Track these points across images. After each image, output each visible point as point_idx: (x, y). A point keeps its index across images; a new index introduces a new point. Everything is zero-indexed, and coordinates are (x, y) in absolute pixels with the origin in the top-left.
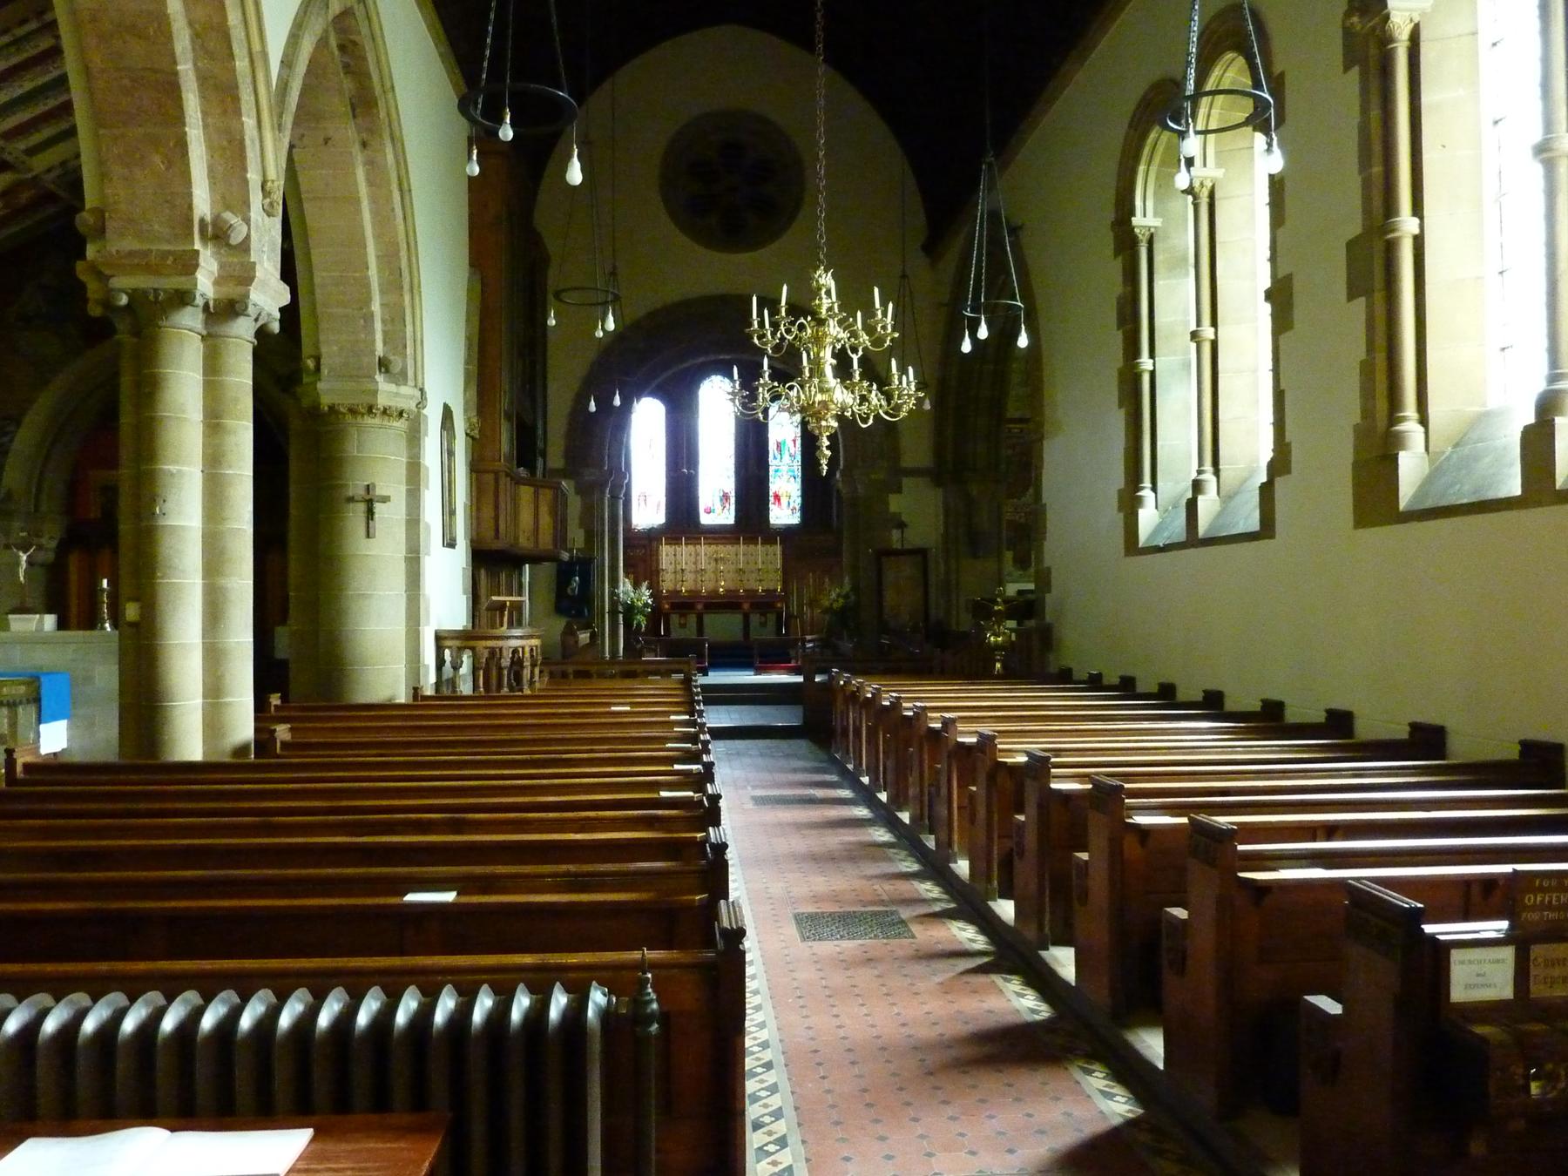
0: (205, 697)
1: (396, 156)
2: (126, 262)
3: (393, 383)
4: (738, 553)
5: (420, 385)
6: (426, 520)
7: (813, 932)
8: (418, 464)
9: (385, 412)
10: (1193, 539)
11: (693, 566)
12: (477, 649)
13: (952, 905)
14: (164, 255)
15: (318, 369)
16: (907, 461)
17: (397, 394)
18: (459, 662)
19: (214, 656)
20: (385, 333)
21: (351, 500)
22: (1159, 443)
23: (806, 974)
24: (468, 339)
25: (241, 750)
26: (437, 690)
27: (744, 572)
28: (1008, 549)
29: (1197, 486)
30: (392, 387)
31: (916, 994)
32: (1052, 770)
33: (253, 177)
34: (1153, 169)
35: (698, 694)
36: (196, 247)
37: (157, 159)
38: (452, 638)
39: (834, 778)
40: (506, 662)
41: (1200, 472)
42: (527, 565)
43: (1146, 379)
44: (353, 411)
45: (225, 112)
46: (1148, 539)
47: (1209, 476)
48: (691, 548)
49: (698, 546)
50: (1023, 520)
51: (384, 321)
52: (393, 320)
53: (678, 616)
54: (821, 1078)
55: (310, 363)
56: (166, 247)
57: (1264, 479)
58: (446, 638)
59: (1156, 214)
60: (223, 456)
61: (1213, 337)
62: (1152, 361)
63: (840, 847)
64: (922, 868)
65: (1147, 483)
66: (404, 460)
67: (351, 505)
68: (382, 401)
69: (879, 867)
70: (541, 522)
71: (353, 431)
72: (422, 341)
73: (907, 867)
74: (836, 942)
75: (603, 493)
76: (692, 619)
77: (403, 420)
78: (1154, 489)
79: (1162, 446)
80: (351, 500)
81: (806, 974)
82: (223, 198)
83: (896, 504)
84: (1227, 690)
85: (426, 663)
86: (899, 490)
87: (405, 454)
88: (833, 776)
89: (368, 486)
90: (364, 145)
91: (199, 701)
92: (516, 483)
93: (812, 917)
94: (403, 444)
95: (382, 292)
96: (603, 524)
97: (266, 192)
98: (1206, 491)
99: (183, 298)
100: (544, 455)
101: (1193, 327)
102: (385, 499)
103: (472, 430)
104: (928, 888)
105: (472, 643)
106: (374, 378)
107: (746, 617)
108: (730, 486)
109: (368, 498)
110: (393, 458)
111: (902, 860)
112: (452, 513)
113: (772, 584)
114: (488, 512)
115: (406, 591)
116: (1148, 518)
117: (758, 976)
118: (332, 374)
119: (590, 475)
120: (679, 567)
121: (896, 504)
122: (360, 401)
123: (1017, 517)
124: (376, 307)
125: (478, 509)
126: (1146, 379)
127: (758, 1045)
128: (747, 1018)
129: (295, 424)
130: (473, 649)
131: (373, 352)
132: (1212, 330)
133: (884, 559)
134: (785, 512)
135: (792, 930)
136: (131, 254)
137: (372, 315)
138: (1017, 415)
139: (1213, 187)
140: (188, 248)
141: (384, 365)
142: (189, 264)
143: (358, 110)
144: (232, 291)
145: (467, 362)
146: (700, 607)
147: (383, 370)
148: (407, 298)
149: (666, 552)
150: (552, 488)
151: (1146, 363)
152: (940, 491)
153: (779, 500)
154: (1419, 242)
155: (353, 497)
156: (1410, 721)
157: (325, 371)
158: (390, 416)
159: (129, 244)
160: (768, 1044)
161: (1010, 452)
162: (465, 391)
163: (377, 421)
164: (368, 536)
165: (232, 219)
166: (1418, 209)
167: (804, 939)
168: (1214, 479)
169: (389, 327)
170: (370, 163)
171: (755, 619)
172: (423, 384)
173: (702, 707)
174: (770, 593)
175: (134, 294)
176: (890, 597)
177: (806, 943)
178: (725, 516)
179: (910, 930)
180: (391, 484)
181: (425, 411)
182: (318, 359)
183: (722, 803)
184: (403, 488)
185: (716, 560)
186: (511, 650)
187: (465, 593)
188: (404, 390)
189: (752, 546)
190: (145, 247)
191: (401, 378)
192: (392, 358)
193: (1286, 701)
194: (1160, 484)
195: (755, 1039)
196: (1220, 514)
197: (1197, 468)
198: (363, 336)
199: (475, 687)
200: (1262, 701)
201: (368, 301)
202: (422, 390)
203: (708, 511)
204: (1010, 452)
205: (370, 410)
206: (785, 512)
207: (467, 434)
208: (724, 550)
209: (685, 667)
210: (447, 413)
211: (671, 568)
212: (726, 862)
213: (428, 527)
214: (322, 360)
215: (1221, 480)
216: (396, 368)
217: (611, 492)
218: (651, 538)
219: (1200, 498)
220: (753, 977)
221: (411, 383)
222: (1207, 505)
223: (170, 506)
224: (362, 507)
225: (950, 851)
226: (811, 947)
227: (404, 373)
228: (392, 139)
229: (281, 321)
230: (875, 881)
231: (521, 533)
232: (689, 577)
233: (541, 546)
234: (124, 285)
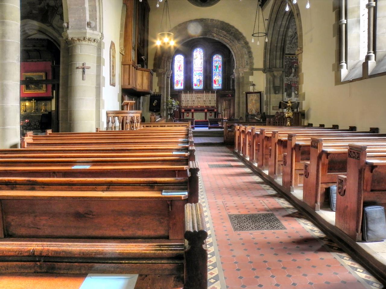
3: (91, 30)
4: (204, 96)
5: (101, 32)
6: (103, 75)
7: (239, 225)
9: (89, 40)
11: (191, 100)
12: (119, 117)
13: (296, 211)
15: (68, 27)
16: (255, 66)
17: (93, 34)
18: (114, 121)
20: (90, 15)
21: (77, 68)
22: (348, 47)
23: (239, 253)
24: (121, 24)
26: (107, 129)
27: (205, 101)
28: (285, 92)
29: (368, 58)
30: (91, 31)
31: (299, 267)
32: (367, 154)
39: (236, 158)
40: (128, 121)
41: (369, 53)
42: (142, 97)
43: (344, 26)
44: (79, 40)
47: (372, 54)
48: (190, 95)
49: (193, 94)
50: (289, 83)
51: (90, 11)
52: (92, 10)
53: (186, 113)
54: (237, 270)
55: (65, 25)
60: (6, 34)
62: (346, 20)
63: (243, 184)
64: (277, 193)
65: (344, 61)
66: (96, 56)
67: (78, 70)
68: (88, 36)
69: (260, 192)
70: (144, 81)
71: (79, 46)
72: (103, 18)
73: (271, 192)
74: (250, 232)
75: (164, 76)
76: (190, 114)
77: (95, 42)
78: (346, 63)
79: (349, 48)
80: (77, 68)
81: (239, 253)
83: (251, 79)
85: (103, 121)
86: (252, 74)
87: (96, 54)
88: (235, 158)
89: (83, 64)
92: (136, 69)
93: (237, 217)
94: (96, 50)
96: (164, 85)
98: (371, 59)
102: (89, 68)
103: (122, 51)
104: (282, 202)
106: (85, 28)
107: (206, 113)
108: (201, 78)
109: (83, 67)
110: (92, 55)
111: (268, 189)
112: (114, 76)
113: (213, 104)
114: (127, 77)
115: (96, 98)
116: (344, 72)
117: (213, 244)
118: (72, 28)
119: (160, 71)
120: (187, 100)
121: (251, 79)
122: (81, 36)
123: (288, 82)
125: (124, 76)
126: (344, 26)
127: (201, 198)
128: (208, 260)
129: (62, 45)
130: (118, 117)
131: (85, 20)
133: (248, 95)
134: (217, 85)
135: (228, 225)
137: (85, 8)
138: (288, 53)
141: (89, 24)
145: (121, 31)
146: (193, 110)
147: (89, 26)
149: (183, 96)
150: (148, 71)
151: (344, 21)
152: (265, 74)
153: (215, 82)
155: (78, 67)
157: (70, 27)
158: (91, 41)
160: (208, 222)
161: (286, 63)
162: (120, 40)
163: (87, 43)
167: (236, 229)
168: (374, 55)
171: (208, 114)
172: (103, 32)
173: (194, 148)
174: (213, 107)
176: (250, 106)
177: (236, 231)
178: (201, 87)
179: (282, 225)
181: (103, 41)
182: (68, 23)
183: (199, 174)
184: (95, 65)
185: (198, 98)
186: (130, 117)
187: (118, 101)
188: (95, 32)
189: (208, 94)
191: (95, 28)
194: (348, 61)
195: (200, 197)
196: (376, 67)
197: (366, 54)
198: (82, 15)
199: (119, 129)
203: (196, 85)
204: (286, 63)
206: (217, 85)
207: (120, 53)
208: (199, 95)
209: (187, 125)
210: (113, 44)
211: (185, 100)
212: (197, 178)
213: (104, 78)
214: (69, 24)
216: (93, 24)
217: (167, 76)
218: (180, 91)
220: (200, 181)
222: (372, 63)
224: (81, 70)
225: (291, 187)
226: (239, 234)
230: (259, 199)
231: (138, 85)
232: (190, 102)
233: (144, 88)
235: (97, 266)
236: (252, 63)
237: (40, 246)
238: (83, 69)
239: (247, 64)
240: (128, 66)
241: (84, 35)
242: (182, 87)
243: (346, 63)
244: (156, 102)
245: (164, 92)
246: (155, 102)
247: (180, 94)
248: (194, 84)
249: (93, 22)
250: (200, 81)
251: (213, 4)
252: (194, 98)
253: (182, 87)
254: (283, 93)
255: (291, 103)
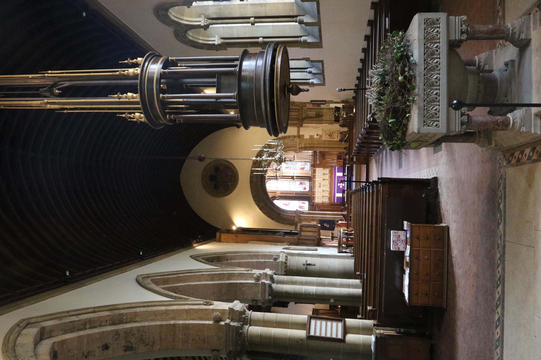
0: (350, 288)
1: (229, 254)
2: (263, 296)
8: (298, 254)
10: (318, 24)
14: (262, 289)
17: (282, 257)
19: (342, 286)
22: (298, 78)
25: (361, 282)
29: (310, 72)
33: (246, 272)
34: (185, 18)
35: (358, 188)
36: (261, 282)
37: (244, 289)
38: (340, 249)
41: (307, 72)
45: (234, 276)
46: (315, 19)
47: (308, 70)
51: (265, 259)
52: (265, 257)
56: (260, 288)
57: (304, 25)
58: (340, 251)
59: (214, 37)
61: (262, 38)
68: (284, 260)
75: (301, 216)
80: (306, 268)
82: (250, 278)
84: (360, 58)
86: (303, 136)
90: (227, 260)
91: (351, 289)
95: (259, 259)
96: (310, 216)
97: (248, 271)
99: (270, 286)
100: (292, 231)
101: (250, 25)
105: (341, 244)
109: (306, 265)
114: (308, 242)
119: (296, 220)
120: (322, 197)
124: (262, 260)
132: (260, 38)
136: (262, 295)
139: (207, 18)
140: (260, 284)
141: (275, 259)
142: (264, 284)
143: (220, 260)
144: (268, 278)
148: (260, 254)
154: (264, 38)
156: (363, 40)
159: (260, 295)
163: (288, 262)
164: (315, 265)
165: (255, 276)
166: (258, 38)
169: (267, 258)
170: (231, 259)
175: (269, 295)
180: (303, 260)
184: (304, 258)
189: (316, 176)
190: (260, 291)
191: (278, 256)
192: (274, 258)
193: (362, 48)
194: (308, 78)
200: (364, 41)
201: (261, 262)
202: (281, 252)
203: (305, 189)
205: (286, 263)
210: (284, 249)
215: (299, 15)
216: (276, 257)
219: (313, 72)
221: (279, 254)
223: (311, 291)
224: (308, 266)
227: (277, 255)
228: (226, 254)
229: (273, 270)
234: (267, 297)
235: (294, 195)
236: (295, 137)
237: (279, 60)
238: (307, 264)
239: (293, 140)
240: (299, 241)
241: (283, 263)
242: (307, 203)
243: (309, 79)
244: (325, 225)
245: (317, 217)
246: (326, 225)
247: (314, 204)
248: (304, 190)
249: (480, 55)
250: (301, 183)
251: (237, 171)
252: (321, 190)
253: (307, 203)
254: (322, 109)
255: (335, 112)
